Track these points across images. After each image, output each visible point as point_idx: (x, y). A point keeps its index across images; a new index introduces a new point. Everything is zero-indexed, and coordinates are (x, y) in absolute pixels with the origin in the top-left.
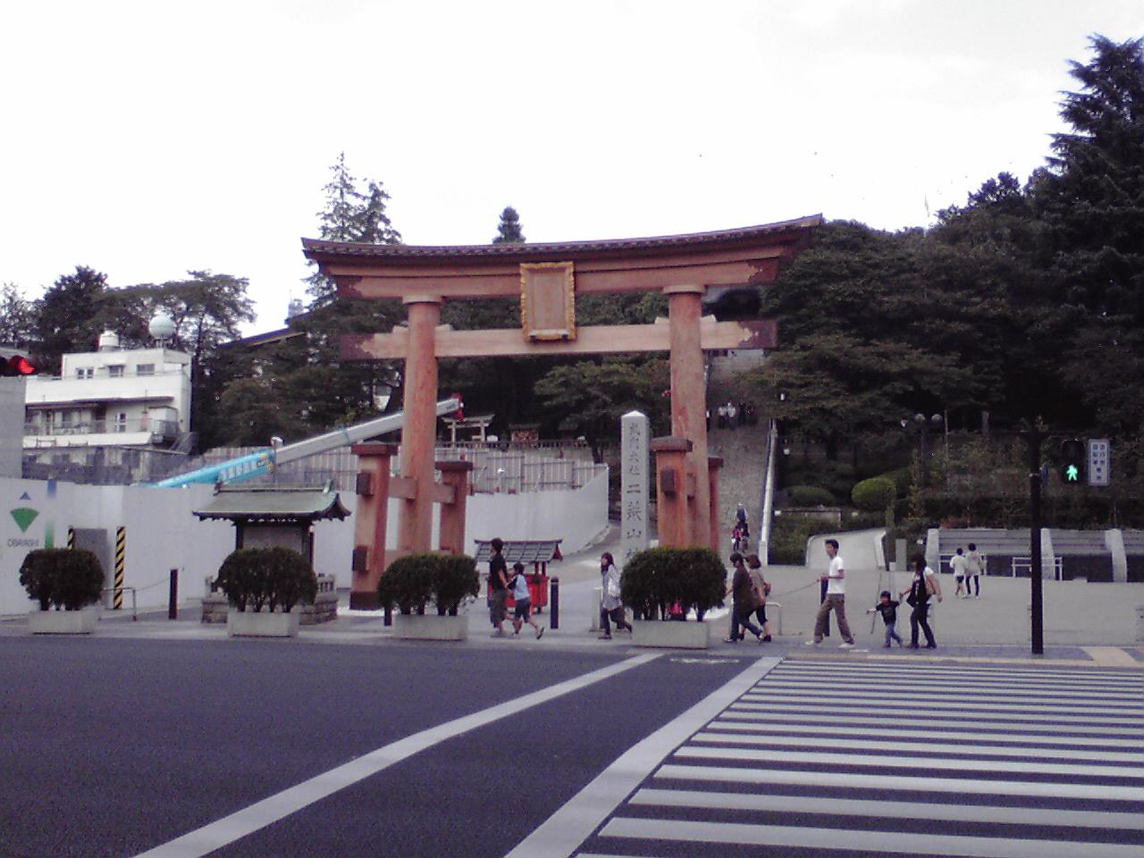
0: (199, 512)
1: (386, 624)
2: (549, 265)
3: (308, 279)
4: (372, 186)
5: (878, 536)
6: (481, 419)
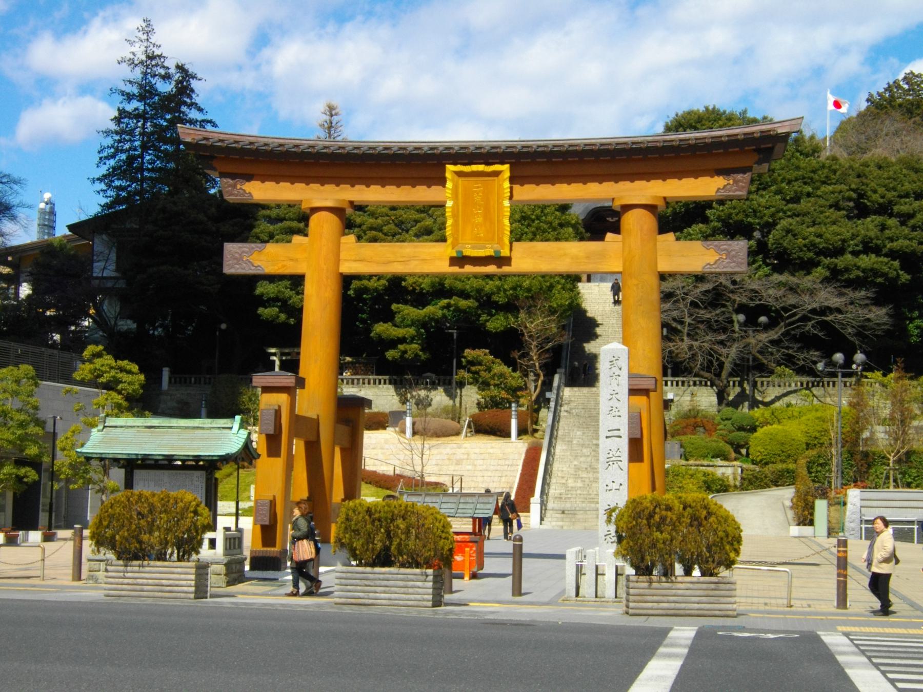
1: (838, 607)
2: (481, 168)
3: (100, 180)
5: (786, 494)
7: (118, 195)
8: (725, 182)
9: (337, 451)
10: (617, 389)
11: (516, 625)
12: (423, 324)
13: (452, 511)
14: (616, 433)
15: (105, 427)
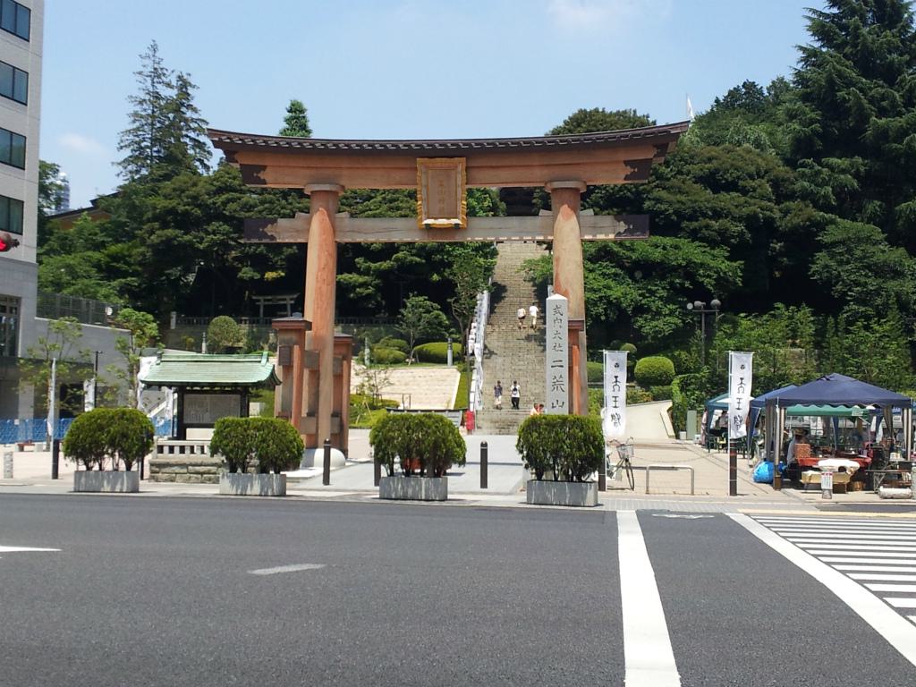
0: (147, 380)
1: (482, 487)
4: (180, 78)
6: (287, 297)
7: (133, 178)
9: (306, 373)
11: (486, 510)
12: (380, 274)
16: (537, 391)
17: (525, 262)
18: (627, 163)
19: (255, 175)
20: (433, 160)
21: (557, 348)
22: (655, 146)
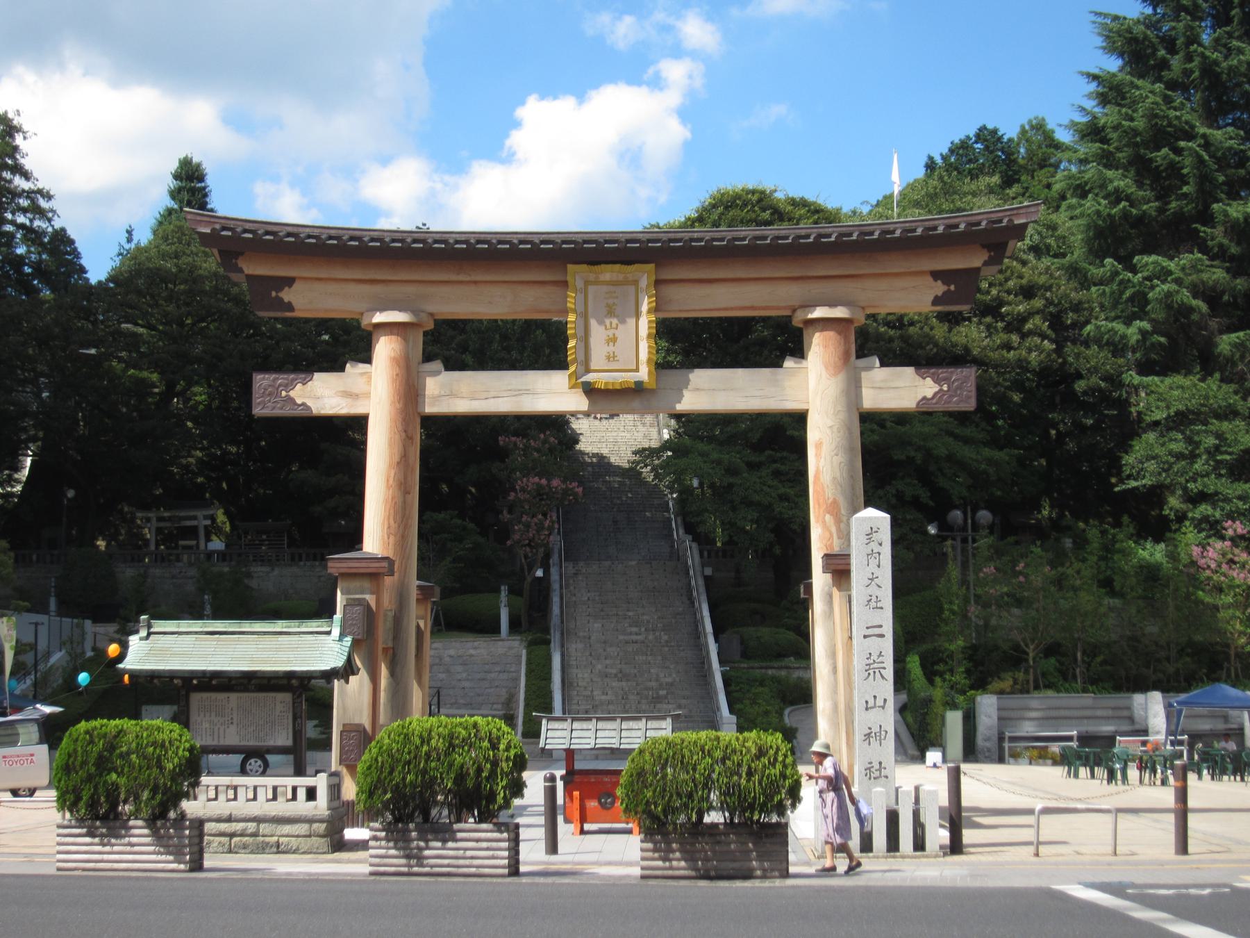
8: (945, 288)
10: (877, 572)
13: (613, 741)
14: (877, 631)
15: (149, 634)
16: (669, 680)
17: (635, 453)
18: (936, 275)
19: (274, 294)
20: (596, 268)
21: (873, 604)
22: (984, 246)
